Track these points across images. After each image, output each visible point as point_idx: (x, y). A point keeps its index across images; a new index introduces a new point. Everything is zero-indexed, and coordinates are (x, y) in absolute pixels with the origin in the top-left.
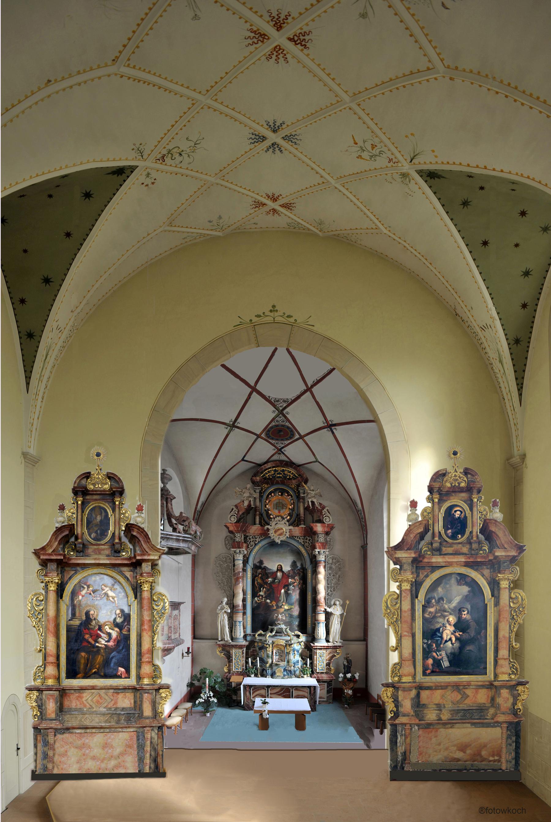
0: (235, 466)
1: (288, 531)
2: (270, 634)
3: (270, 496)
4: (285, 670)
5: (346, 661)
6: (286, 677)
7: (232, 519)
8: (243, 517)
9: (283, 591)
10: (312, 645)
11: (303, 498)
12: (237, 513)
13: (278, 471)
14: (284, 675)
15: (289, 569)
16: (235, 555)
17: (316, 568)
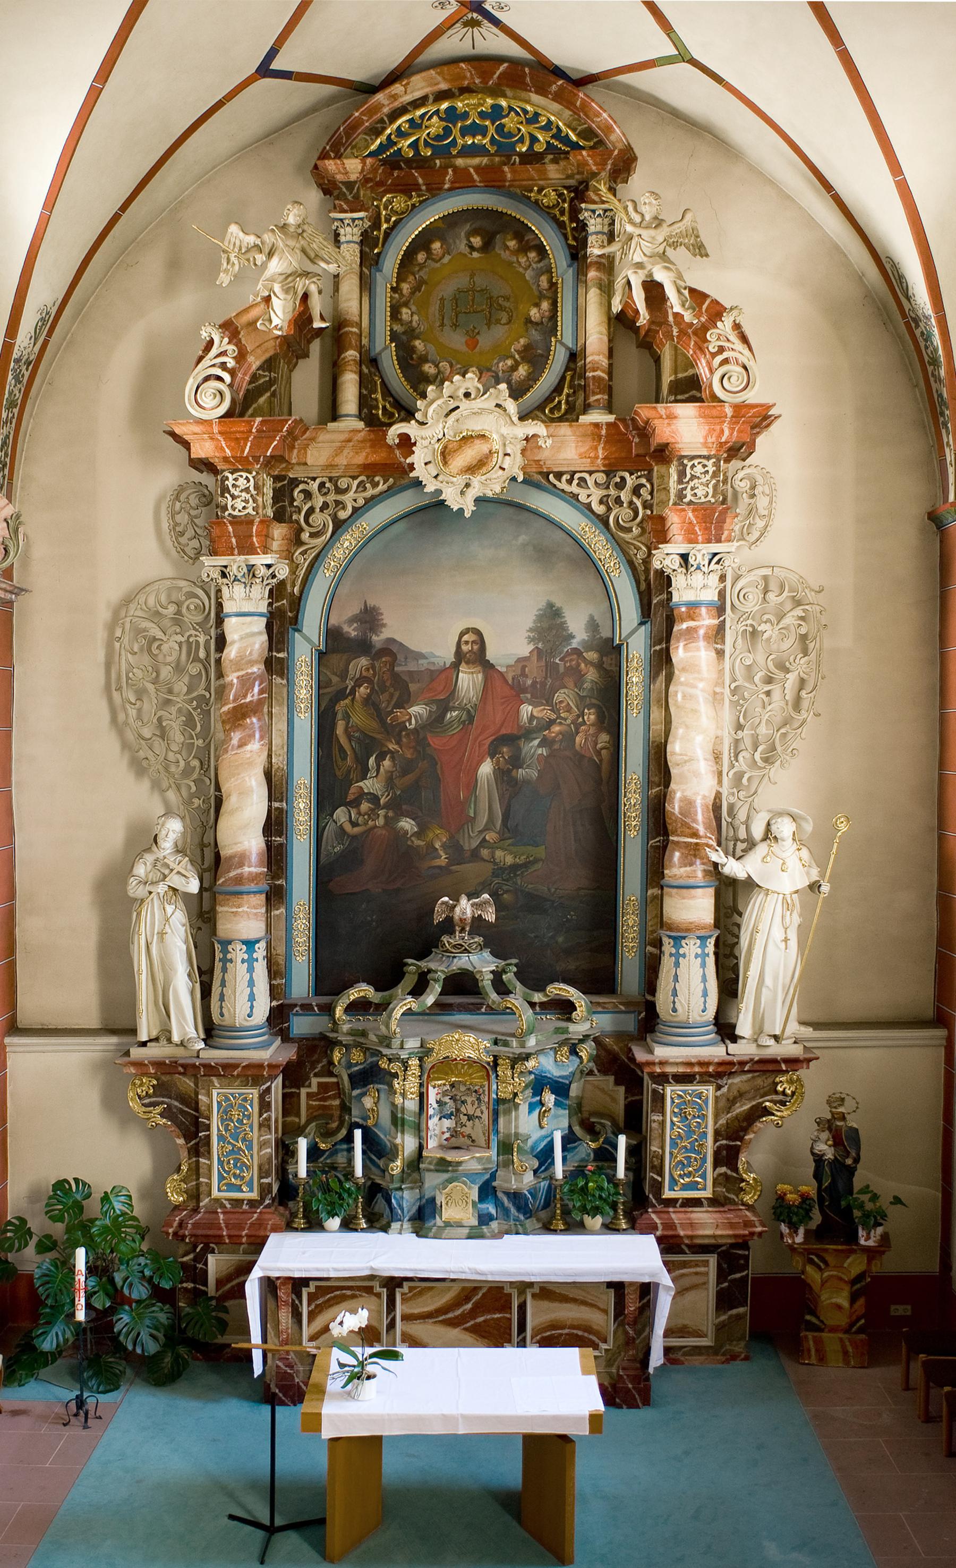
0: (219, 105)
1: (515, 449)
2: (410, 1003)
3: (421, 257)
4: (487, 1191)
5: (825, 1135)
6: (494, 1225)
7: (208, 399)
8: (271, 382)
9: (486, 769)
10: (640, 1055)
11: (608, 265)
12: (231, 363)
13: (465, 115)
14: (484, 1219)
15: (524, 649)
16: (225, 590)
17: (668, 641)
